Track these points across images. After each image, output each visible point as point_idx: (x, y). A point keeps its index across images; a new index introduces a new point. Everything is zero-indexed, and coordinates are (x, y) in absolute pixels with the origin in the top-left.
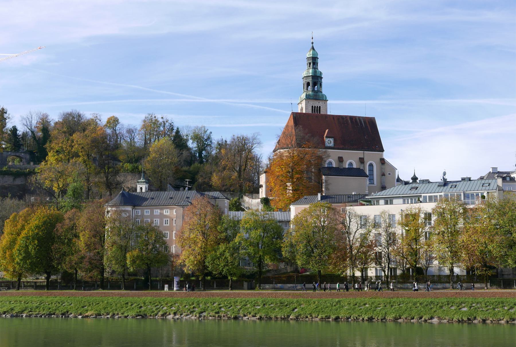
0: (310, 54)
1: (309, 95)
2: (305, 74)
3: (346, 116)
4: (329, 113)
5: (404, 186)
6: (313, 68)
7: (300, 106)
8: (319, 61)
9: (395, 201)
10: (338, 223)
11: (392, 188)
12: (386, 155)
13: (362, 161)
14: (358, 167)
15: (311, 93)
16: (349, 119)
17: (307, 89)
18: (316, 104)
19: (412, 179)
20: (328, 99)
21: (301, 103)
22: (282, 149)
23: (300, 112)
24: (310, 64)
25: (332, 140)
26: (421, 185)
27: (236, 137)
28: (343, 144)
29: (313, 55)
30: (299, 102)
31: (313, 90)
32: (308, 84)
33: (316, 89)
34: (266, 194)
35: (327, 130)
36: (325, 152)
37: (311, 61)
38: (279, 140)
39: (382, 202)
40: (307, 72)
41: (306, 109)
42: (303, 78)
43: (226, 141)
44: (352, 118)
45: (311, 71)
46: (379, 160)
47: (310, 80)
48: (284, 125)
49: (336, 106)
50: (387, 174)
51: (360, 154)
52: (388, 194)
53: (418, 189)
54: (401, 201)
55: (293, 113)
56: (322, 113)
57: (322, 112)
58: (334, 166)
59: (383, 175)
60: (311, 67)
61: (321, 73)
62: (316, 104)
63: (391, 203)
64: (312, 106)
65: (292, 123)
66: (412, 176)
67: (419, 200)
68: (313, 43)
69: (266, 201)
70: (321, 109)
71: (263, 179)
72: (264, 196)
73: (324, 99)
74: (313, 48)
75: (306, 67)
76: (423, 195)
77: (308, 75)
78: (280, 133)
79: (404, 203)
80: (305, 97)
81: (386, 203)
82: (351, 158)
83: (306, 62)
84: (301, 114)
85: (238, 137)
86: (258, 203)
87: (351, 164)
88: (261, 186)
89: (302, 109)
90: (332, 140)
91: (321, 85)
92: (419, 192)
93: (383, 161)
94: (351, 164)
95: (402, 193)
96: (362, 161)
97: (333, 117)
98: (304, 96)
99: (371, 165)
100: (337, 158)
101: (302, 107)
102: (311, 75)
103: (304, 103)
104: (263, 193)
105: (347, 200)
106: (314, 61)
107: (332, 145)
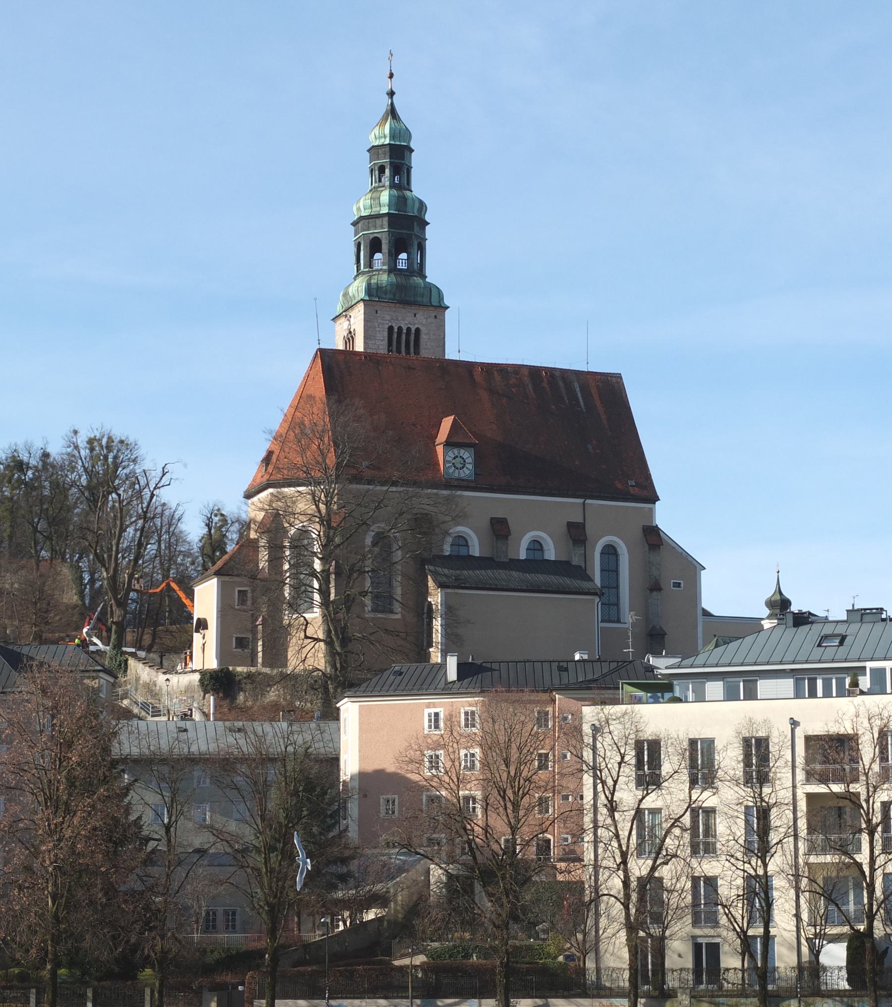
0: (381, 135)
1: (379, 288)
2: (362, 206)
3: (517, 369)
4: (451, 353)
5: (791, 631)
6: (393, 186)
7: (342, 327)
8: (417, 161)
9: (764, 686)
10: (585, 768)
11: (749, 640)
12: (667, 517)
13: (577, 534)
14: (563, 558)
15: (384, 278)
16: (526, 380)
17: (370, 264)
18: (406, 319)
19: (770, 604)
20: (447, 302)
21: (345, 313)
22: (290, 486)
23: (341, 347)
24: (382, 169)
25: (467, 455)
26: (854, 627)
27: (82, 440)
28: (508, 466)
29: (393, 136)
30: (339, 309)
31: (393, 269)
32: (375, 246)
33: (402, 265)
34: (223, 653)
35: (447, 423)
36: (448, 499)
37: (385, 161)
38: (270, 454)
39: (715, 688)
40: (371, 199)
41: (366, 337)
42: (354, 224)
43: (46, 455)
44: (535, 372)
45: (385, 196)
46: (639, 533)
47: (381, 230)
48: (286, 399)
49: (477, 333)
50: (668, 583)
51: (569, 507)
52: (738, 659)
53: (848, 641)
54: (788, 684)
55: (320, 350)
56: (425, 353)
57: (427, 351)
58: (551, 554)
59: (656, 587)
60: (386, 180)
61: (422, 206)
62: (406, 319)
63: (751, 695)
64: (391, 329)
65: (319, 388)
66: (769, 592)
67: (855, 684)
68: (391, 94)
69: (219, 683)
70: (424, 337)
71: (206, 600)
72: (212, 664)
73: (435, 301)
74: (392, 112)
75: (366, 181)
76: (869, 665)
77: (375, 210)
78: (275, 421)
79: (798, 695)
80: (362, 295)
81: (731, 695)
82: (538, 524)
83: (365, 163)
84: (348, 354)
85: (91, 441)
86: (188, 689)
87: (536, 546)
88: (202, 624)
89: (350, 338)
90: (467, 455)
91: (422, 248)
92: (854, 654)
93: (653, 537)
94: (536, 546)
95: (789, 657)
96: (577, 534)
97: (468, 367)
98: (358, 288)
99: (610, 552)
100: (485, 523)
101: (351, 331)
102: (385, 210)
103: (358, 316)
104: (205, 652)
105: (556, 681)
106: (395, 160)
107: (468, 471)
